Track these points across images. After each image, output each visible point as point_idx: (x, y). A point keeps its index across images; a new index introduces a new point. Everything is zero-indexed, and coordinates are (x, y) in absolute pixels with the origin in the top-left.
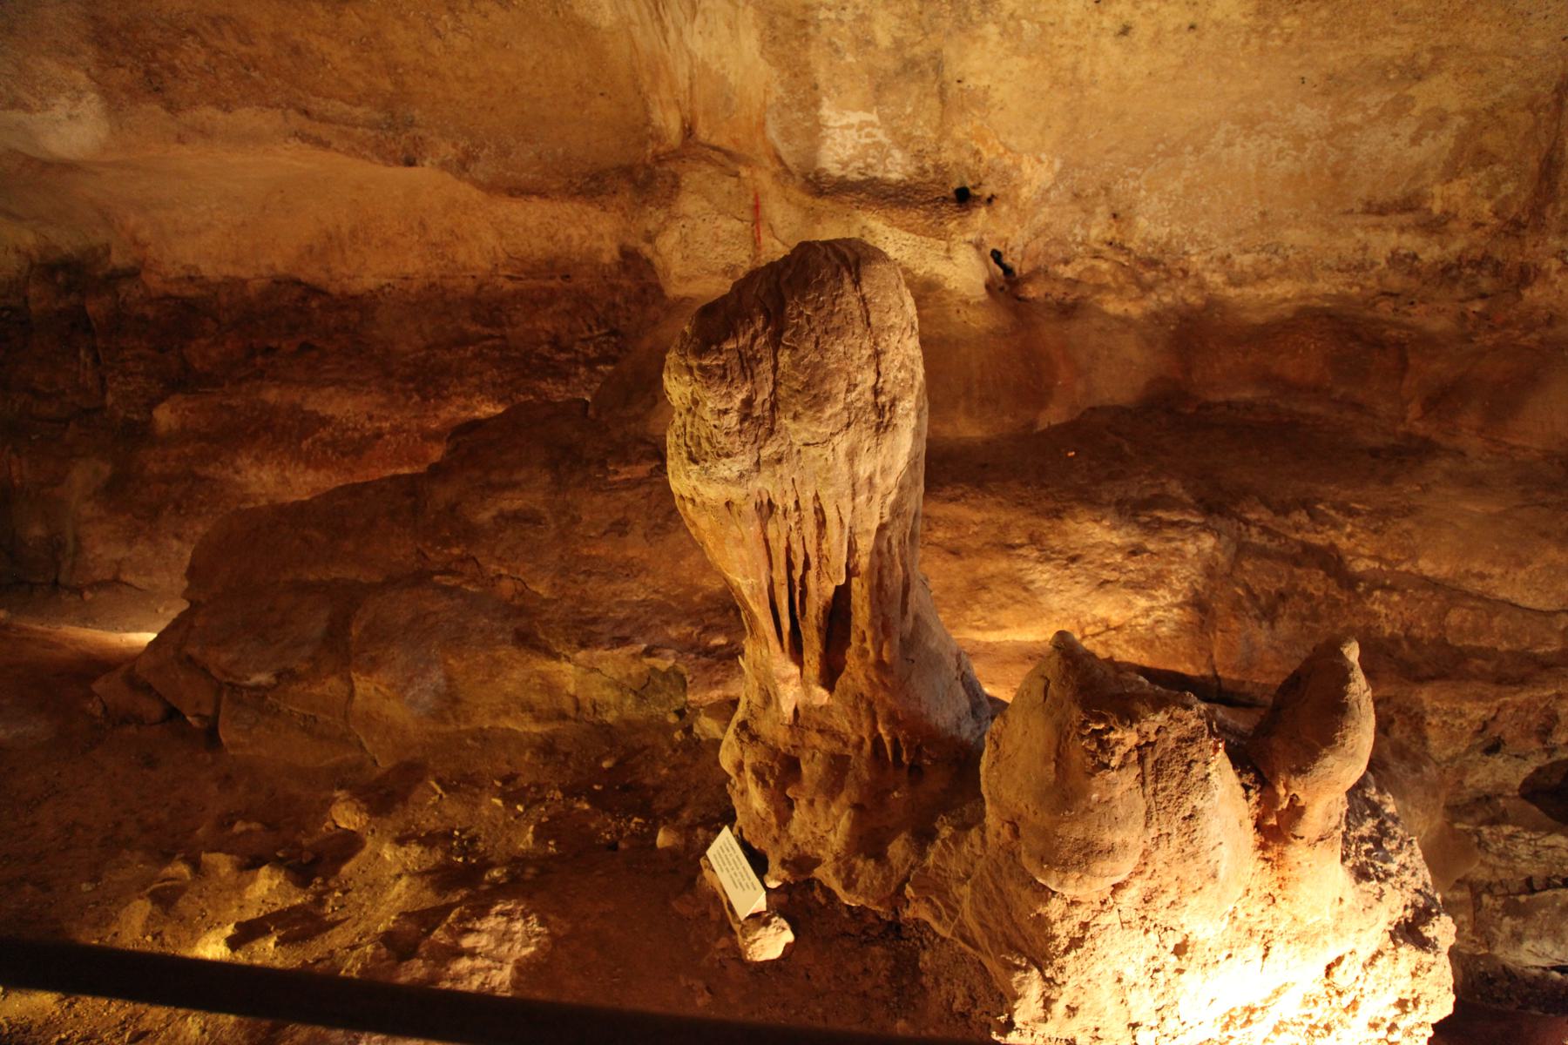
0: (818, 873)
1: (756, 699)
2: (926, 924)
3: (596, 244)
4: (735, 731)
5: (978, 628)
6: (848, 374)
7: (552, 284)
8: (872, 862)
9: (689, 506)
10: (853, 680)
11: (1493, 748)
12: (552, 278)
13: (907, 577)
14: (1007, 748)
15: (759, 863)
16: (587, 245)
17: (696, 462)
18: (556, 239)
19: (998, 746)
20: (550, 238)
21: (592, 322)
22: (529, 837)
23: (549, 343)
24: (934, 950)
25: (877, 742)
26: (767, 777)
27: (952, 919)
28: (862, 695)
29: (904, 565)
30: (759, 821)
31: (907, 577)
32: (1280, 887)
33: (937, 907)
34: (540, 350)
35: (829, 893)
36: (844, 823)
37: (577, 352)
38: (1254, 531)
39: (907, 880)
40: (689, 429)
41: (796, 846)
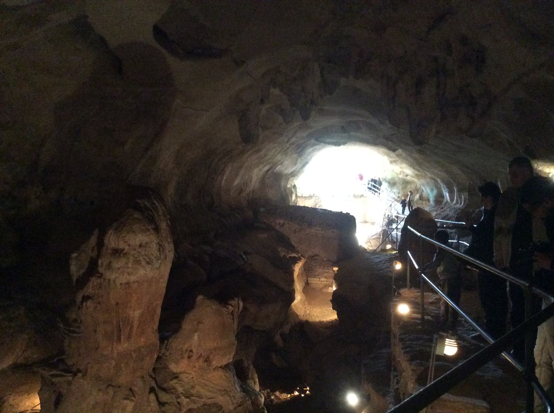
26: (131, 398)
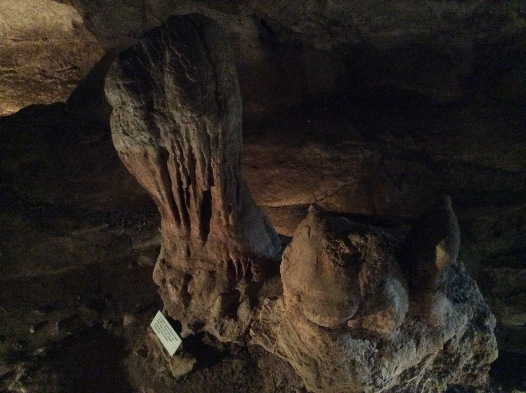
0: (207, 328)
1: (169, 248)
2: (261, 347)
3: (60, 21)
4: (160, 265)
5: (268, 201)
6: (203, 85)
7: (37, 43)
8: (232, 321)
9: (126, 157)
10: (217, 235)
11: (497, 235)
12: (37, 40)
13: (238, 183)
14: (293, 261)
15: (177, 326)
16: (54, 21)
17: (127, 134)
18: (37, 19)
19: (288, 261)
20: (34, 18)
21: (63, 63)
22: (57, 328)
23: (40, 74)
24: (265, 358)
25: (230, 262)
27: (274, 344)
28: (221, 242)
29: (236, 178)
30: (175, 307)
31: (238, 183)
32: (421, 312)
33: (265, 338)
34: (35, 78)
35: (213, 338)
36: (218, 303)
37: (55, 78)
38: (389, 146)
39: (250, 327)
40: (121, 118)
41: (194, 317)
